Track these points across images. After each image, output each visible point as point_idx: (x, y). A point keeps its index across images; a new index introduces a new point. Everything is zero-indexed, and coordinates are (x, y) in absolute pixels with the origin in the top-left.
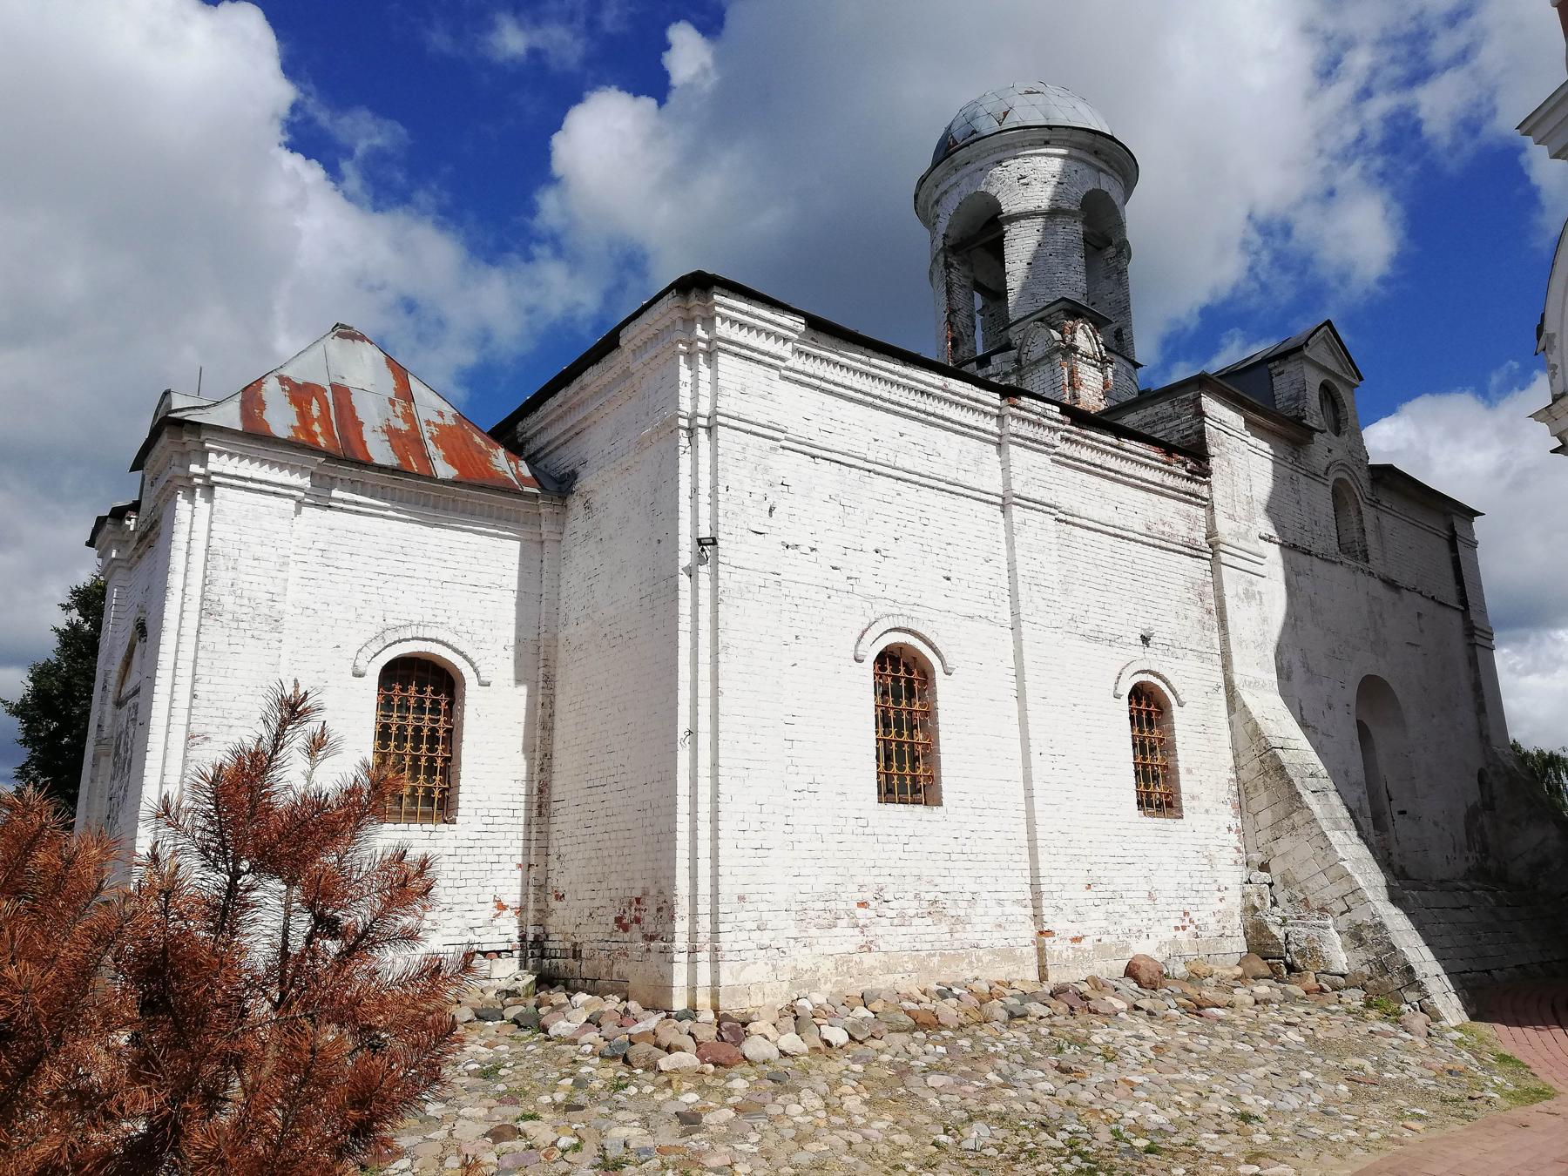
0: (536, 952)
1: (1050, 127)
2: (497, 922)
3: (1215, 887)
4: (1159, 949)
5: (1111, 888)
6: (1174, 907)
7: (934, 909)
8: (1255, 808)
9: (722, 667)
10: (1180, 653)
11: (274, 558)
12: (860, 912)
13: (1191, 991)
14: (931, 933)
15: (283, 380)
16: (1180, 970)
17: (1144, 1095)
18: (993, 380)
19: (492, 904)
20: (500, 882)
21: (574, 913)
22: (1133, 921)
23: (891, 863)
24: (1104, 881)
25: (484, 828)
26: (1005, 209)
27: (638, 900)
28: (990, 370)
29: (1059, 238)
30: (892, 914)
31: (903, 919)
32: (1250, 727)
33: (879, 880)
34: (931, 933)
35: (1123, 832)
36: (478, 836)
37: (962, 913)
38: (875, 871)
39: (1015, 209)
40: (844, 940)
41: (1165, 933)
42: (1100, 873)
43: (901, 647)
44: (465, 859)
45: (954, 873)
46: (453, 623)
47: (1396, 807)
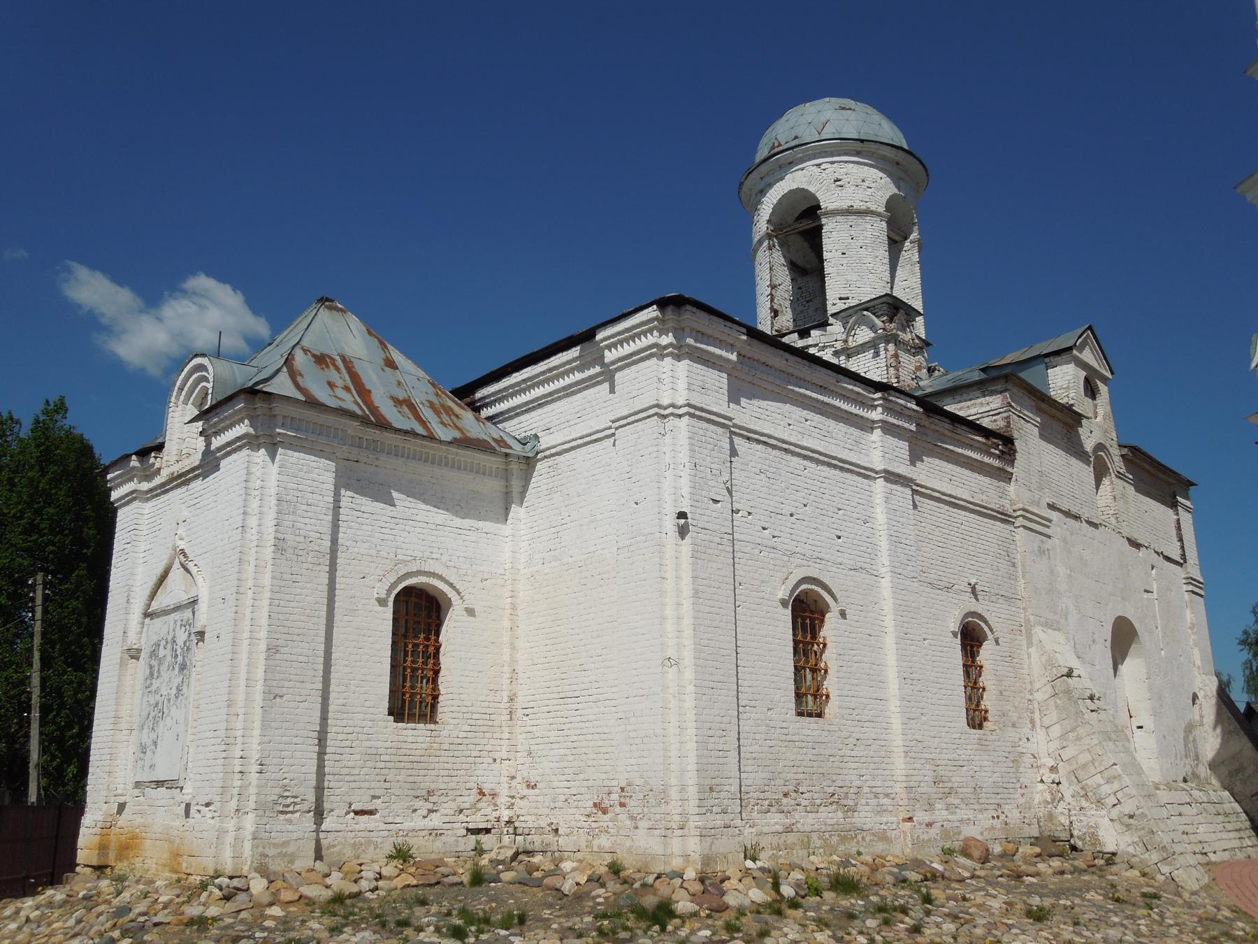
0: (511, 831)
1: (862, 141)
2: (480, 805)
3: (1018, 785)
4: (982, 834)
5: (950, 785)
6: (992, 801)
7: (833, 800)
8: (1047, 721)
9: (326, 529)
10: (994, 599)
11: (321, 504)
12: (785, 801)
13: (1010, 865)
14: (830, 816)
15: (305, 351)
16: (997, 849)
17: (1017, 931)
18: (812, 351)
19: (475, 791)
20: (480, 772)
21: (548, 799)
22: (964, 813)
23: (804, 763)
24: (945, 779)
25: (469, 728)
26: (823, 205)
27: (622, 789)
28: (810, 341)
29: (868, 234)
30: (807, 803)
31: (814, 808)
32: (1044, 658)
33: (797, 776)
34: (830, 816)
35: (957, 741)
36: (464, 735)
37: (851, 803)
38: (795, 769)
39: (831, 207)
40: (775, 820)
41: (985, 820)
42: (943, 773)
43: (806, 592)
44: (456, 753)
45: (845, 771)
46: (445, 559)
47: (1135, 722)
